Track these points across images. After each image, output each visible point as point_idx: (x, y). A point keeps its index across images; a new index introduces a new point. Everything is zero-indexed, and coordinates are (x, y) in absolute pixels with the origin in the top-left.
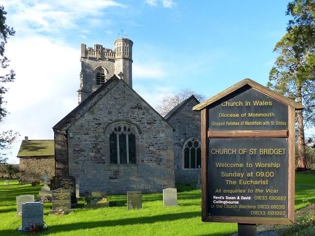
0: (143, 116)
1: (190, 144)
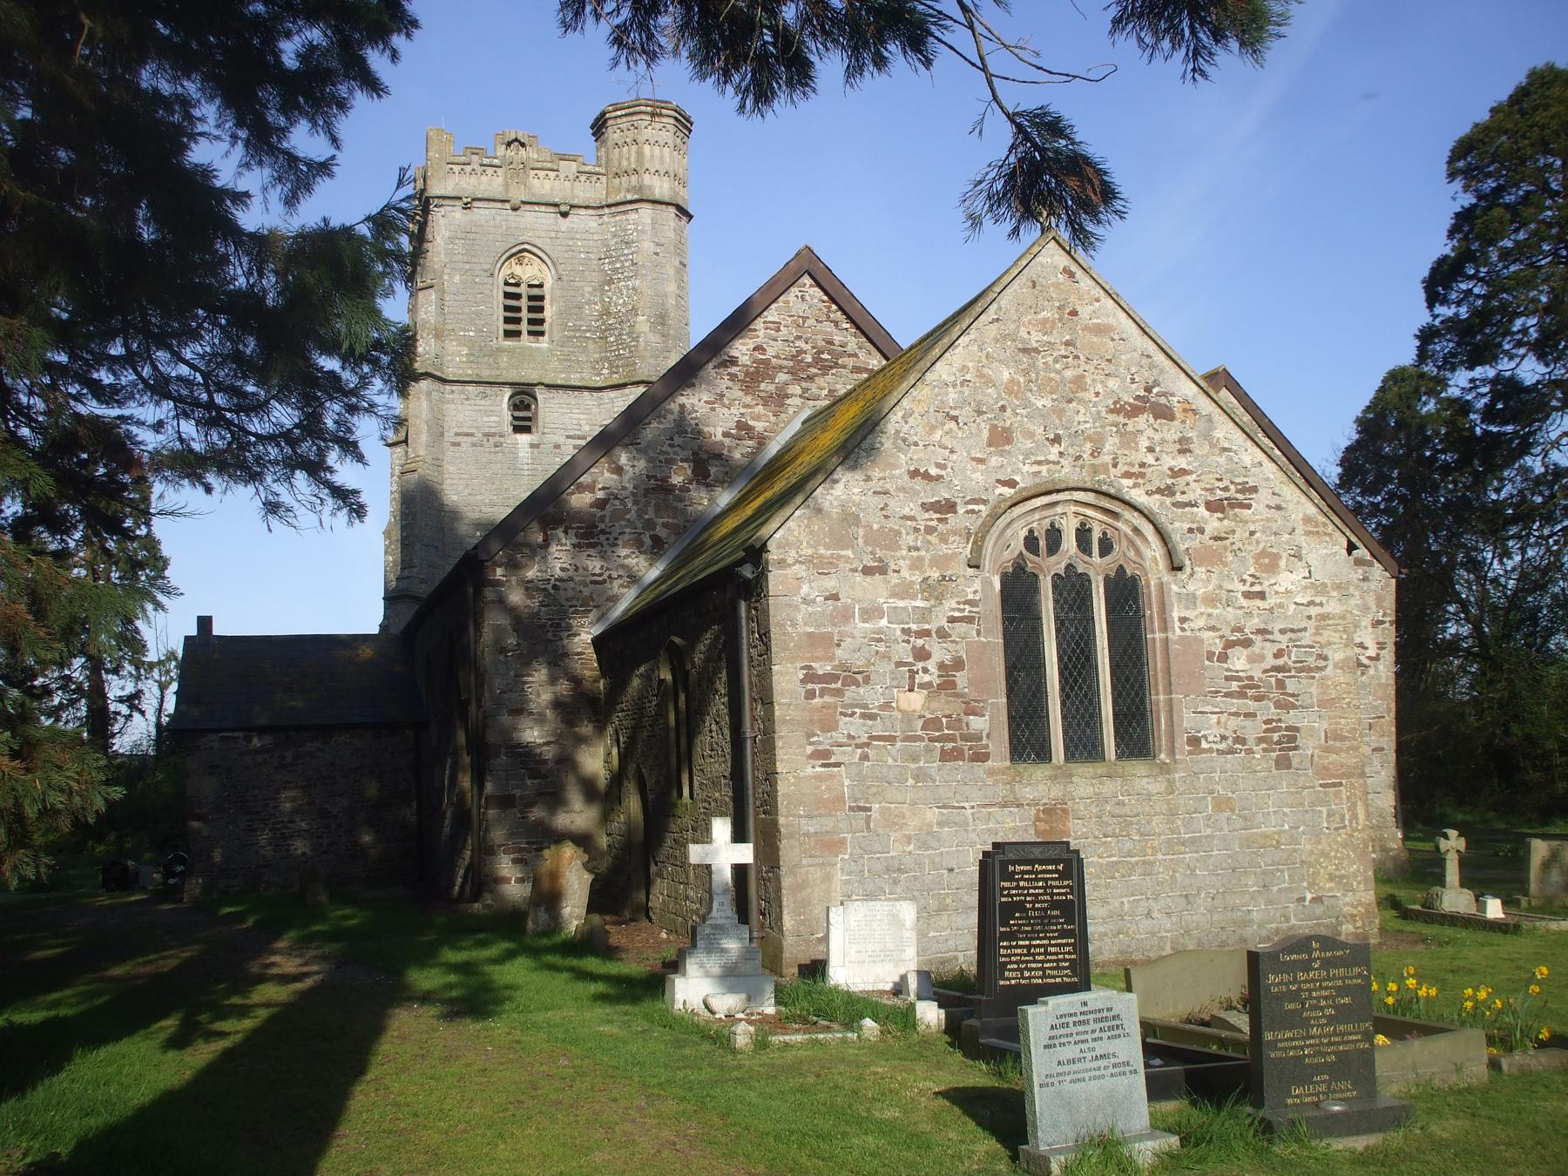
0: (1182, 462)
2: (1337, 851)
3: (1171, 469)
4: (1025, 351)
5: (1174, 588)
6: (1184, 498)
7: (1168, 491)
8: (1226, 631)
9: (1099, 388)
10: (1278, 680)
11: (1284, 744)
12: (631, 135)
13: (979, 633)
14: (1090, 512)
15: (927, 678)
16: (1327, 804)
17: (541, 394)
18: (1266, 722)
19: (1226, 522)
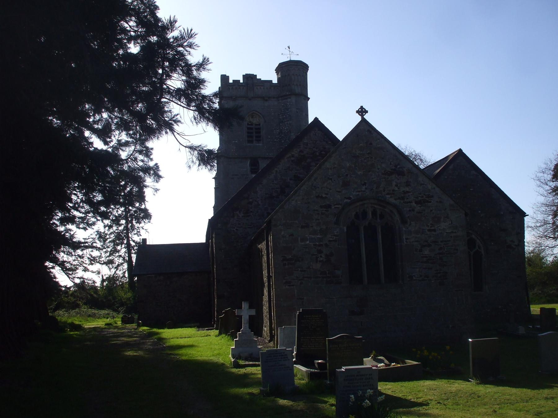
0: (407, 189)
15: (322, 259)
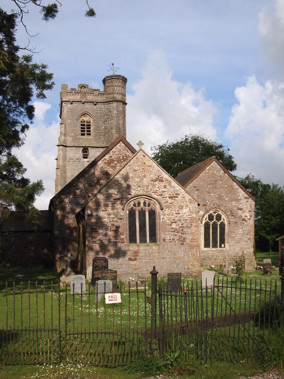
0: (164, 190)
1: (211, 217)
2: (193, 260)
3: (162, 191)
4: (135, 171)
5: (161, 213)
6: (165, 196)
7: (161, 195)
8: (171, 220)
9: (149, 177)
10: (182, 229)
11: (182, 241)
12: (111, 84)
13: (123, 221)
14: (146, 199)
15: (114, 229)
16: (191, 251)
17: (89, 149)
18: (179, 237)
19: (173, 200)
